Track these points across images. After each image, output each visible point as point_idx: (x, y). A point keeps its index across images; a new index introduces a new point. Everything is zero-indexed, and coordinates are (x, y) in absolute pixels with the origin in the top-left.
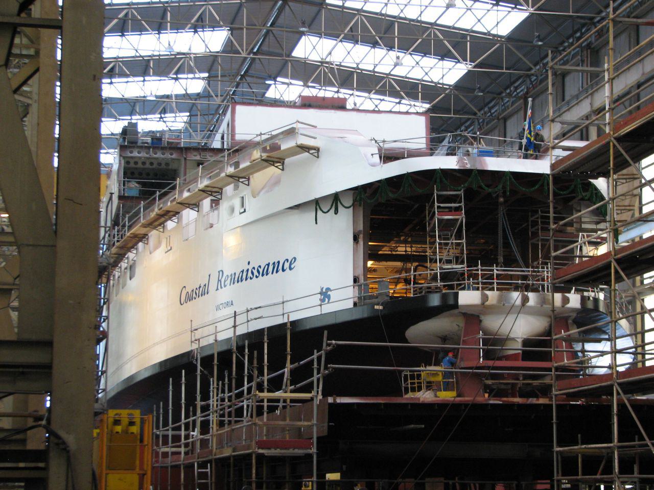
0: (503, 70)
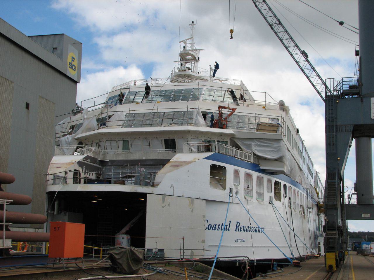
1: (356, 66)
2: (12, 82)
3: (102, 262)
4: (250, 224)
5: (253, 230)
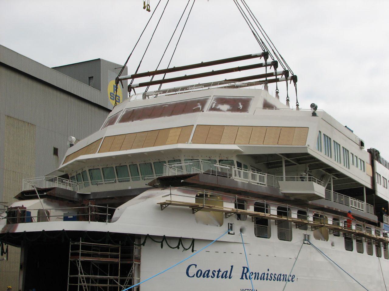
0: (69, 283)
1: (262, 60)
2: (32, 124)
4: (268, 270)
5: (273, 278)
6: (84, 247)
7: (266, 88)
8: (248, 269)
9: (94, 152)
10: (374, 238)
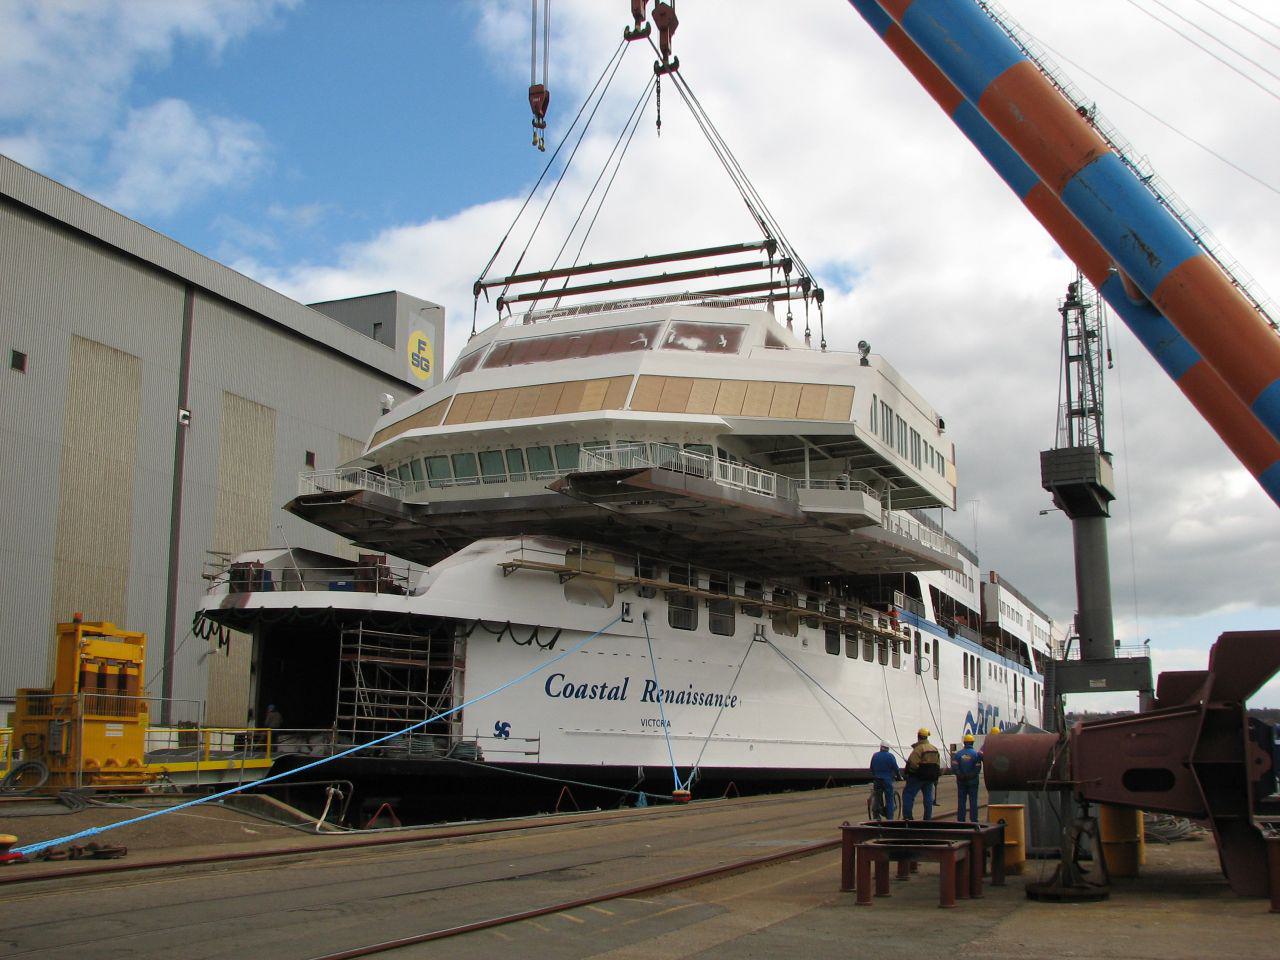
1: (762, 256)
3: (235, 785)
6: (367, 639)
7: (771, 308)
8: (655, 685)
9: (435, 423)
10: (876, 633)
